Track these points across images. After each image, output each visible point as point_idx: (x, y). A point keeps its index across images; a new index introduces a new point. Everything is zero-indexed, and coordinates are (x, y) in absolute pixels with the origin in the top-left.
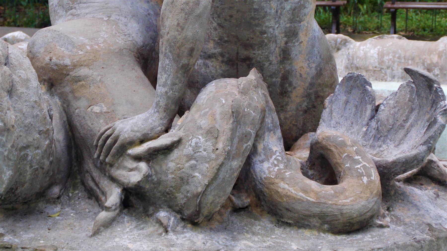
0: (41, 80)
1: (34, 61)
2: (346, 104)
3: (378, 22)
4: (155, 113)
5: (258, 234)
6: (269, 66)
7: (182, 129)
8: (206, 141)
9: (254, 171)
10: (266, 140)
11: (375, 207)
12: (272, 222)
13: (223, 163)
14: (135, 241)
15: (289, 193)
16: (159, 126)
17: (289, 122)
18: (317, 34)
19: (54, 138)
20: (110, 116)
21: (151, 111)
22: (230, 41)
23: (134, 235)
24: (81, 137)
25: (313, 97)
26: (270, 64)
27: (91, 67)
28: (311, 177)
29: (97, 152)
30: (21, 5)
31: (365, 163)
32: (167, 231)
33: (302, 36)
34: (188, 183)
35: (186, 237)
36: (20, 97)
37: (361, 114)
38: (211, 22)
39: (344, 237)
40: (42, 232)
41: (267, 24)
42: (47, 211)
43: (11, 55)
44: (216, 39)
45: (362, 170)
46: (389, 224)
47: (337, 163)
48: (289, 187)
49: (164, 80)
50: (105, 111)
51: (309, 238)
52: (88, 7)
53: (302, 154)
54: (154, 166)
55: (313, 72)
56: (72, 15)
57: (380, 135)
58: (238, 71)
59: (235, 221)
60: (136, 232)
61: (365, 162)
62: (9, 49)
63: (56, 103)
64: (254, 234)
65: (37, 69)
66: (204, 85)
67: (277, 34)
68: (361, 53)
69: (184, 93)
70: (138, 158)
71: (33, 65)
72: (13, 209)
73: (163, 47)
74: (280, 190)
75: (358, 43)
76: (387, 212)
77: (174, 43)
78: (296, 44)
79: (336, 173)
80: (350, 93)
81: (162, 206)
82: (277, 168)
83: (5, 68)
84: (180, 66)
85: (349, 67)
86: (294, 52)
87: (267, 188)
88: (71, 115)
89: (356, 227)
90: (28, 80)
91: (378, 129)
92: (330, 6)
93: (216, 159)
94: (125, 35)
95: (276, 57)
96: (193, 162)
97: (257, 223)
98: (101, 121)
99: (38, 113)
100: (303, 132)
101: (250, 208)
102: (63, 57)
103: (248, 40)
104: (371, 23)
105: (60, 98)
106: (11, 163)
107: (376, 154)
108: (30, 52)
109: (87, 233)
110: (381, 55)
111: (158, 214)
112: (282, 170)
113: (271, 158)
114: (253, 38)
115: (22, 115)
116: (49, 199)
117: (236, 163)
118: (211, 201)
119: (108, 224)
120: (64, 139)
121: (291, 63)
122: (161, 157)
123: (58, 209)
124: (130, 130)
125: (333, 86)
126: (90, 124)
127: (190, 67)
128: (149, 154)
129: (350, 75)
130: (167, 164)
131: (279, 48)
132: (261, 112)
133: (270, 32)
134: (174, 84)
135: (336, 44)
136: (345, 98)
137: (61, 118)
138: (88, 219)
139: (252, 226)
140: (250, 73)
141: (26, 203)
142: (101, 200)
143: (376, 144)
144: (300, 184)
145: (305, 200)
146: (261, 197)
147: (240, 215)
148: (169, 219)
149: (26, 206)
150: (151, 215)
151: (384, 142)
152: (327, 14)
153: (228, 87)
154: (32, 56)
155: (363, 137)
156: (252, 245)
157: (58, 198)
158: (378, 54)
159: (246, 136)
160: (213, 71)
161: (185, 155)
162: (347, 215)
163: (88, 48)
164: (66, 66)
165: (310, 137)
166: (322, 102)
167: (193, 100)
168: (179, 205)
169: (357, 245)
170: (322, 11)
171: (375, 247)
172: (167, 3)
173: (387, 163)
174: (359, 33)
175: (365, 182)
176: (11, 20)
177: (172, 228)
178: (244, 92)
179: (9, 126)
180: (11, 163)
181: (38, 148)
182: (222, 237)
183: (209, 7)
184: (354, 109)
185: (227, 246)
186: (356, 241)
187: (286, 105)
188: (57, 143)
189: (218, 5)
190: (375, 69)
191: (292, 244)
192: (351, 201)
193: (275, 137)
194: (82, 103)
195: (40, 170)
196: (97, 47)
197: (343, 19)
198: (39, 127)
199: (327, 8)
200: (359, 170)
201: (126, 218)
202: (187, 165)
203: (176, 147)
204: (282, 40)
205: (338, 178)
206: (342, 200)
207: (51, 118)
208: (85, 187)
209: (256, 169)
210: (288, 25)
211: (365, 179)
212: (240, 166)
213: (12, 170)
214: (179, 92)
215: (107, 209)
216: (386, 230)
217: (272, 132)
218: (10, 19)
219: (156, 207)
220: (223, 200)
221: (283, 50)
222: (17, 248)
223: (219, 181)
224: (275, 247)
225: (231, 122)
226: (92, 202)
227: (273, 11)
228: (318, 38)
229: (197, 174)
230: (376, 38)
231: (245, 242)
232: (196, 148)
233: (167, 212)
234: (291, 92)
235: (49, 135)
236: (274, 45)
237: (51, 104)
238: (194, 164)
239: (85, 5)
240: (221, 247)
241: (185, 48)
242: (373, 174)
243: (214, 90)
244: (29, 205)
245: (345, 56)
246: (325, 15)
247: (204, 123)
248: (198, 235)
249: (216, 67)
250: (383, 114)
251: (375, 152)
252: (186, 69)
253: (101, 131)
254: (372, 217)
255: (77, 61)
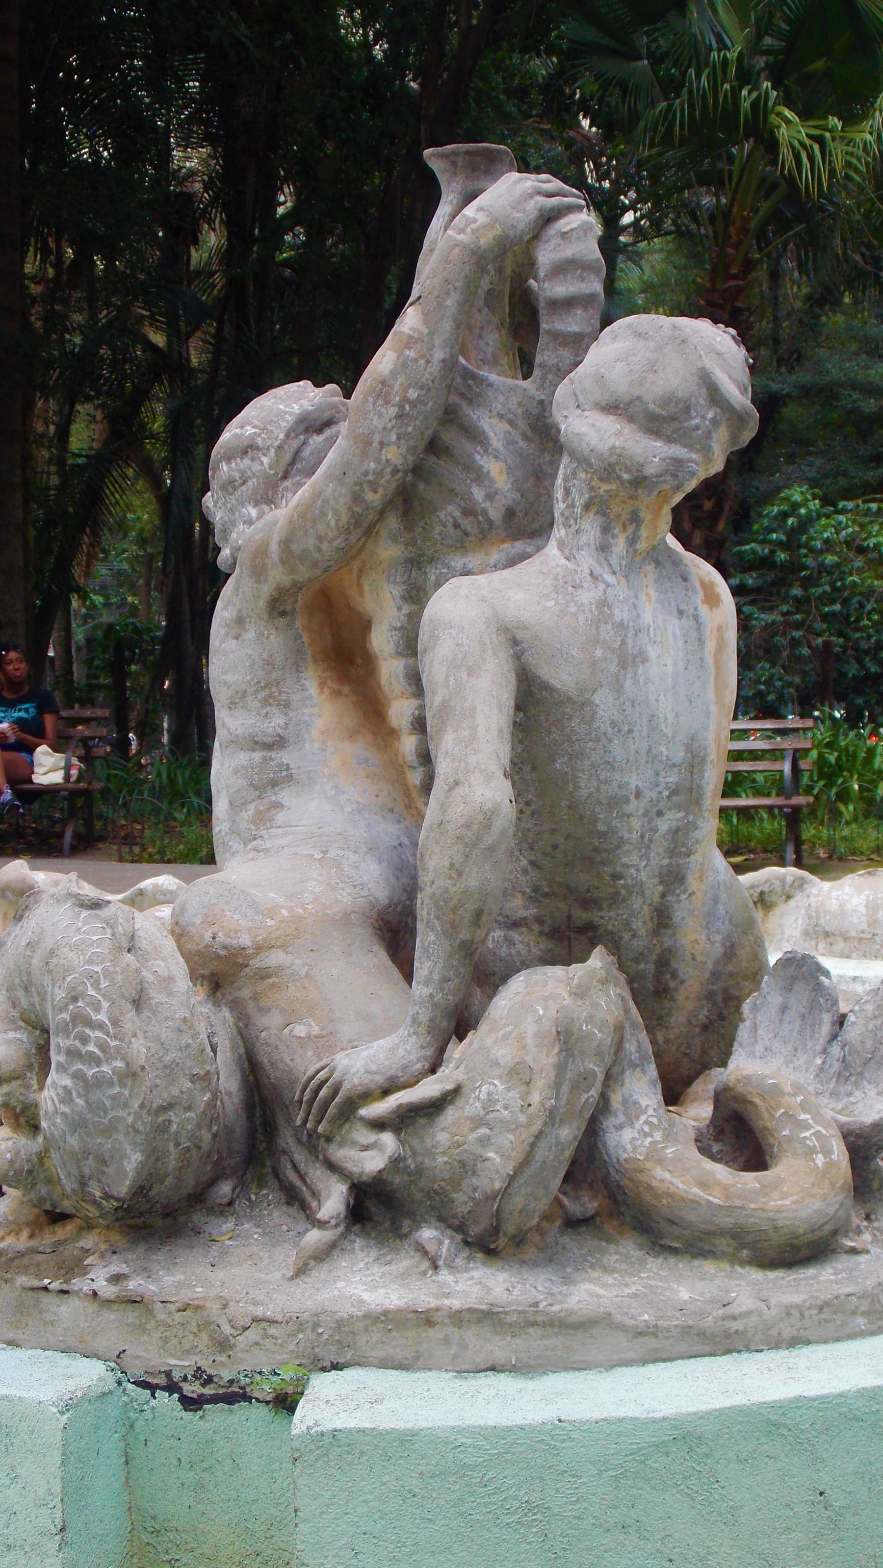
0: (195, 976)
1: (183, 940)
2: (783, 1012)
3: (878, 839)
4: (409, 1035)
5: (613, 1270)
6: (630, 940)
7: (462, 1067)
8: (508, 1089)
9: (605, 1145)
10: (627, 1085)
11: (842, 1213)
12: (641, 1247)
13: (541, 1132)
14: (375, 1287)
15: (672, 1189)
16: (418, 1061)
17: (673, 1049)
18: (723, 877)
19: (221, 1088)
20: (326, 1042)
21: (402, 1032)
22: (554, 894)
23: (373, 1275)
24: (272, 1084)
25: (719, 998)
26: (634, 936)
27: (290, 949)
28: (713, 1157)
29: (302, 1114)
30: (175, 819)
31: (819, 1128)
32: (436, 1267)
33: (692, 882)
34: (474, 1172)
35: (472, 1278)
36: (155, 1012)
37: (813, 1032)
38: (518, 859)
39: (780, 1273)
40: (199, 1270)
41: (624, 860)
42: (208, 1228)
43: (139, 933)
44: (528, 890)
45: (814, 1142)
46: (869, 1247)
47: (766, 1128)
48: (673, 1176)
49: (426, 972)
50: (315, 1033)
51: (712, 1279)
52: (286, 835)
53: (700, 1111)
54: (410, 1139)
55: (718, 950)
56: (255, 850)
57: (849, 1072)
58: (570, 951)
59: (568, 1246)
60: (376, 1269)
61: (819, 1125)
62: (136, 920)
63: (224, 1022)
64: (605, 1270)
65: (187, 956)
66: (504, 979)
67: (644, 879)
68: (833, 905)
69: (469, 995)
70: (378, 1125)
71: (180, 948)
72: (145, 1226)
73: (424, 908)
74: (654, 1183)
75: (827, 885)
76: (865, 1223)
77: (444, 901)
78: (683, 897)
79: (765, 1148)
80: (791, 990)
81: (426, 1217)
82: (649, 1139)
83: (129, 957)
84: (456, 944)
85: (811, 931)
86: (679, 914)
87: (632, 1180)
88: (253, 1044)
89: (804, 1253)
90: (170, 979)
91: (844, 1060)
92: (780, 808)
93: (529, 1125)
94: (355, 886)
95: (645, 923)
96: (484, 1131)
97: (612, 1248)
98: (310, 1054)
99: (190, 1041)
100: (703, 1066)
101: (598, 1219)
102: (236, 932)
103: (588, 891)
104: (865, 840)
105: (232, 1010)
106: (138, 1139)
107: (843, 1109)
108: (177, 923)
109: (284, 1272)
110: (872, 907)
111: (418, 1234)
112: (658, 1143)
113: (637, 1119)
114: (598, 888)
115: (159, 1047)
116: (212, 1207)
117: (566, 1132)
118: (520, 1207)
119: (323, 1255)
120: (240, 1090)
121: (674, 935)
122: (422, 1121)
123: (230, 1225)
124: (363, 1070)
125: (759, 977)
126: (288, 1060)
127: (475, 946)
128: (399, 1117)
129: (789, 955)
130: (434, 1136)
131: (650, 905)
132: (615, 1031)
133: (631, 875)
134: (445, 979)
135: (783, 886)
136: (780, 1000)
137: (234, 1049)
138: (286, 1245)
139: (603, 1255)
140: (593, 955)
141: (169, 1214)
142: (310, 1208)
143: (842, 1089)
144: (693, 1172)
145: (703, 1202)
146: (619, 1198)
147: (579, 1234)
148: (441, 1243)
149: (169, 1221)
150: (406, 1236)
151: (857, 1085)
152: (776, 823)
153: (550, 983)
154: (179, 933)
155: (817, 1076)
156: (601, 1291)
157: (230, 1204)
158: (867, 906)
159: (586, 1078)
160: (522, 952)
161: (467, 1118)
162: (786, 1231)
163: (285, 912)
164: (244, 948)
165: (718, 1077)
166: (738, 1008)
167: (484, 1008)
168: (460, 1215)
169: (807, 1289)
170: (765, 816)
171: (840, 1292)
172: (431, 826)
173: (863, 1127)
174: (832, 862)
175: (820, 1165)
176: (155, 850)
177: (446, 1259)
178: (580, 993)
179: (136, 1068)
180: (138, 1139)
181: (189, 1108)
182: (543, 1277)
183: (511, 831)
184: (798, 1022)
185: (552, 1295)
186: (803, 1282)
187: (667, 1015)
188: (226, 1098)
189: (529, 826)
190: (862, 935)
191: (681, 1288)
192: (794, 1202)
193: (645, 1079)
194: (273, 1020)
195: (194, 1151)
196: (300, 911)
197: (808, 831)
198: (190, 1068)
199: (776, 811)
200: (808, 1142)
201: (359, 1243)
202: (472, 1137)
203: (452, 1102)
204: (654, 890)
205: (768, 1158)
206: (775, 1201)
207: (214, 1050)
208: (280, 1181)
209: (608, 1144)
210: (666, 862)
211: (820, 1160)
212: (575, 1138)
213: (142, 1152)
214: (454, 995)
215: (322, 1224)
216: (862, 1258)
217: (638, 1069)
218: (154, 847)
219: (414, 1221)
220: (544, 1204)
221: (657, 910)
222: (153, 1302)
223: (534, 1168)
224: (646, 1295)
225: (556, 1051)
226: (293, 1211)
227: (635, 835)
228: (725, 885)
229: (491, 1155)
230: (862, 875)
231: (587, 1286)
232: (490, 1103)
233: (436, 1228)
234: (677, 990)
235: (209, 1083)
236: (640, 900)
237: (215, 1022)
238: (484, 1135)
239: (280, 831)
240: (541, 1297)
241: (466, 910)
242: (835, 1148)
243: (522, 990)
244: (175, 1219)
245: (803, 911)
246: (772, 824)
247: (504, 1054)
248: (498, 1273)
249: (528, 945)
250: (853, 1032)
251: (840, 1106)
252: (467, 950)
253: (309, 1073)
254: (835, 1233)
255: (264, 939)
